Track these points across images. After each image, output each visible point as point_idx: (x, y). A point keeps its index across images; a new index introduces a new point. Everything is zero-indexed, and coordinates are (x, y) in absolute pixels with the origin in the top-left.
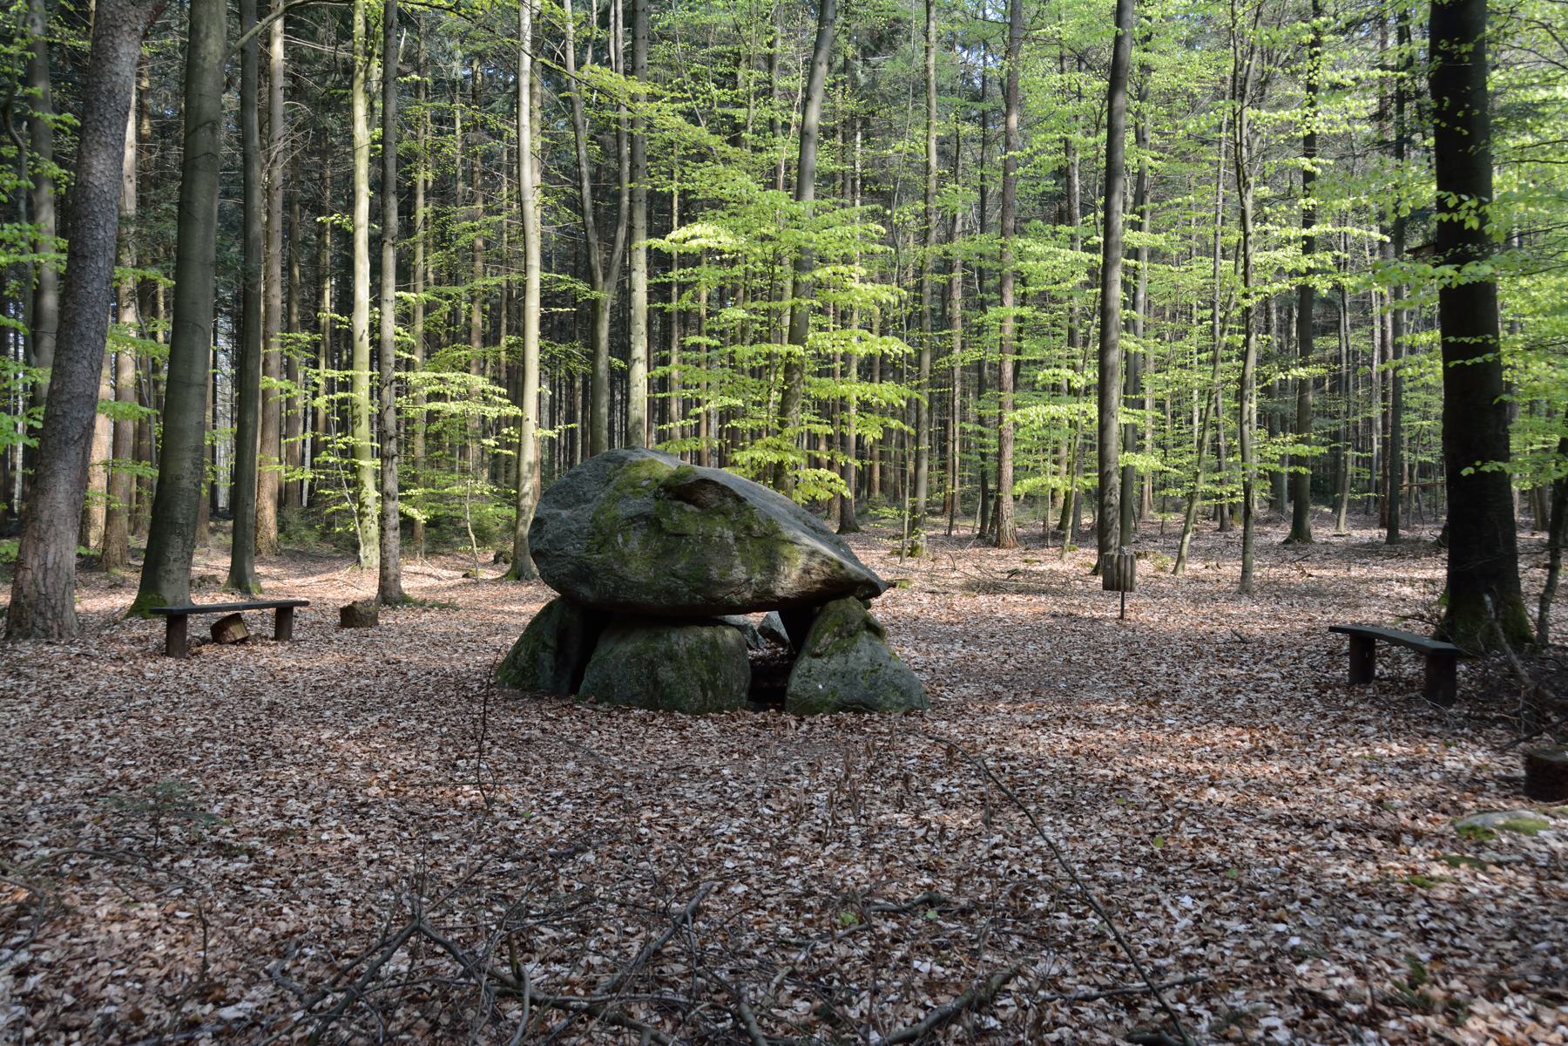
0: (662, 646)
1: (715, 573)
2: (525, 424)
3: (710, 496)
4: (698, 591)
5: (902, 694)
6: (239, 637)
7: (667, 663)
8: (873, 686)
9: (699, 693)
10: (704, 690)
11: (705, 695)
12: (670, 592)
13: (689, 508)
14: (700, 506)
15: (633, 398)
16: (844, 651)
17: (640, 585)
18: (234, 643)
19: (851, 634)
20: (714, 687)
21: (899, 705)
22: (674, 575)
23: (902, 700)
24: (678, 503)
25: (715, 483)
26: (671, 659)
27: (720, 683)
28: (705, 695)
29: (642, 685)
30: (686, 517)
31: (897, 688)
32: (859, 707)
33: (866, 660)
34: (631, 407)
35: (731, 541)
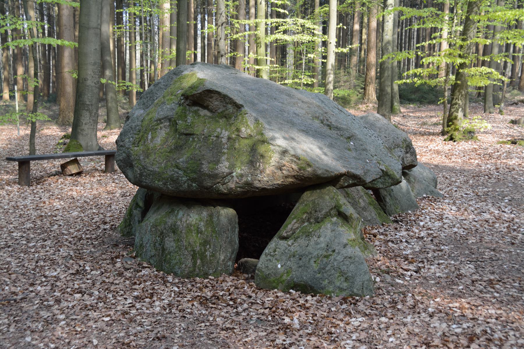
0: (170, 221)
1: (206, 168)
2: (329, 45)
3: (215, 103)
4: (193, 180)
5: (346, 279)
6: (74, 172)
7: (172, 235)
8: (322, 270)
9: (189, 263)
10: (194, 257)
11: (195, 264)
12: (174, 180)
13: (203, 112)
14: (211, 111)
15: (386, 28)
16: (308, 235)
17: (154, 173)
18: (72, 175)
19: (318, 221)
20: (203, 257)
21: (341, 290)
22: (177, 167)
23: (345, 285)
24: (196, 108)
25: (218, 93)
26: (174, 232)
27: (208, 253)
28: (195, 264)
29: (156, 250)
30: (201, 123)
31: (342, 273)
32: (305, 289)
33: (323, 245)
34: (384, 34)
35: (224, 140)
